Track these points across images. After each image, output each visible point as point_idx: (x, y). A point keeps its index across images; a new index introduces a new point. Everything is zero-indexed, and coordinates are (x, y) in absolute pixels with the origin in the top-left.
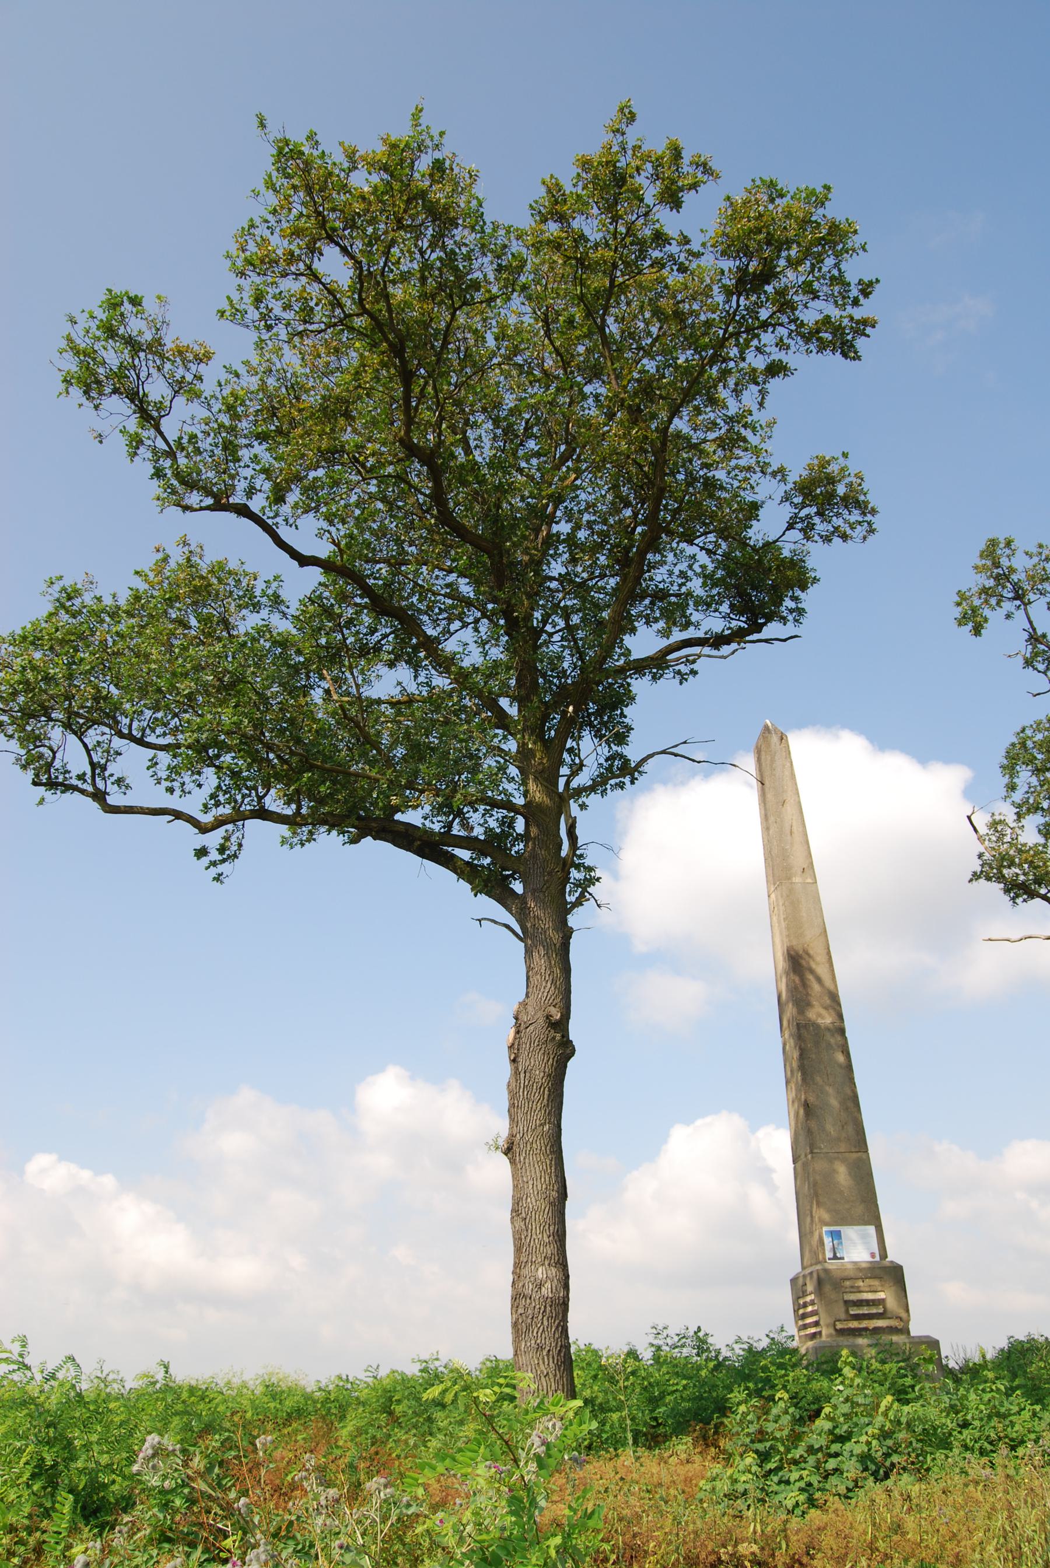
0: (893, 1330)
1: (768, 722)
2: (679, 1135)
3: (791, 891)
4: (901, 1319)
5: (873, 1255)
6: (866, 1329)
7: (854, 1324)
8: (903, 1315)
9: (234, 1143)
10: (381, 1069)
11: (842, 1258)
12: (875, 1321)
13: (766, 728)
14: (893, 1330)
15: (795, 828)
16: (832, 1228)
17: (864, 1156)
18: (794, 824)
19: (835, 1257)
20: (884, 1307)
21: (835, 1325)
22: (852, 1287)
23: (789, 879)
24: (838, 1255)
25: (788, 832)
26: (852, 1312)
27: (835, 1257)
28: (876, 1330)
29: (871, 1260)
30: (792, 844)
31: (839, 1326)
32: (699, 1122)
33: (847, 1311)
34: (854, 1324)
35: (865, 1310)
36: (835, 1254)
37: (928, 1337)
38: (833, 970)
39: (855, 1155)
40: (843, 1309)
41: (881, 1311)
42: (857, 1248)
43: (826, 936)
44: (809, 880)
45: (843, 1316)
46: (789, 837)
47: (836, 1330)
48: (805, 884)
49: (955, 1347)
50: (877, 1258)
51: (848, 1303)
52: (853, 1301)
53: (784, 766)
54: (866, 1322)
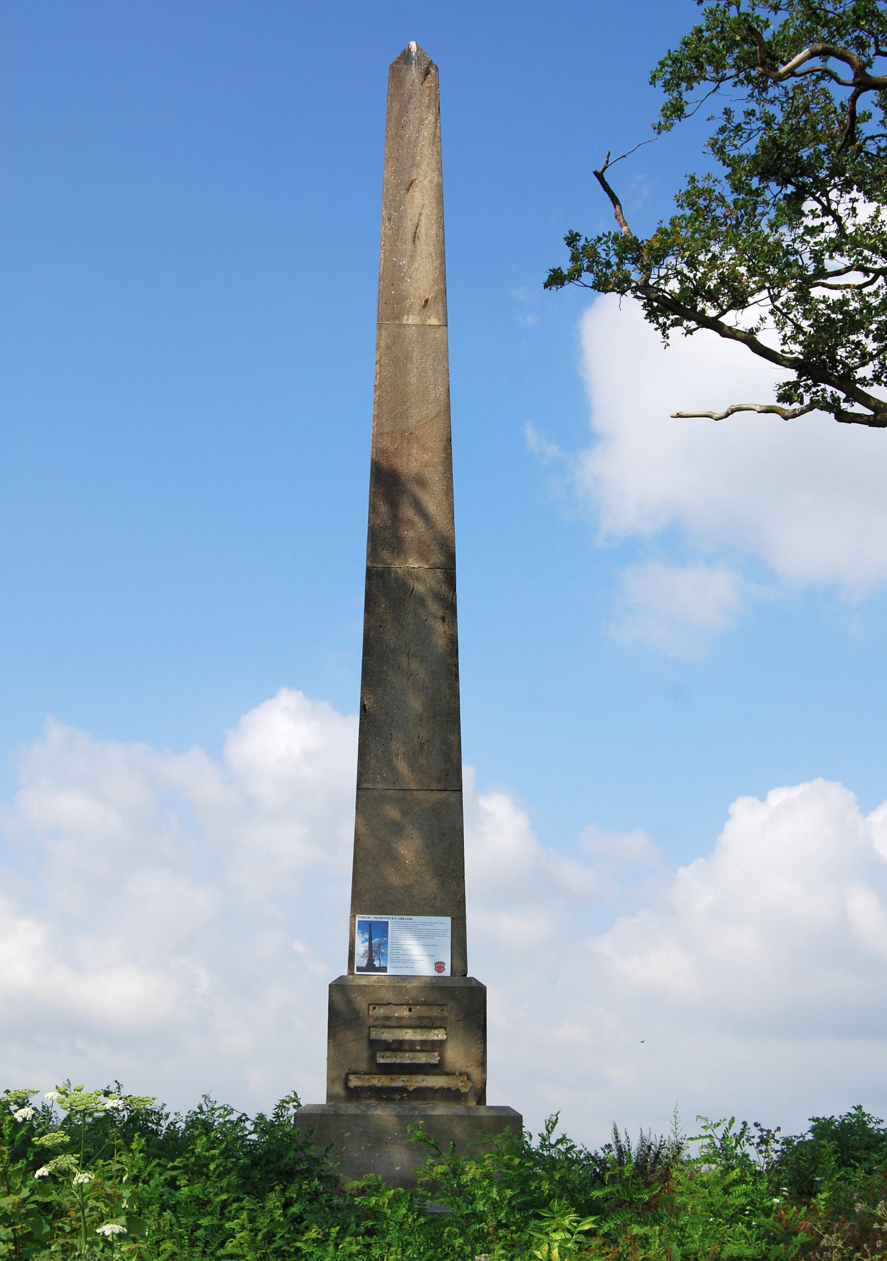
0: (451, 1095)
1: (413, 45)
2: (746, 818)
3: (396, 339)
4: (468, 1076)
5: (439, 966)
6: (402, 1090)
7: (378, 1081)
8: (474, 1071)
9: (71, 807)
10: (267, 693)
11: (384, 969)
12: (420, 1078)
13: (406, 56)
14: (451, 1095)
15: (422, 230)
16: (372, 918)
17: (453, 798)
18: (423, 223)
19: (370, 967)
20: (441, 1056)
21: (346, 1080)
22: (387, 1018)
23: (398, 317)
24: (377, 963)
25: (409, 237)
26: (381, 1061)
27: (370, 967)
28: (422, 1093)
29: (436, 974)
30: (412, 257)
31: (354, 1082)
32: (778, 797)
33: (372, 1058)
34: (378, 1081)
35: (406, 1058)
36: (371, 961)
37: (507, 1109)
38: (450, 478)
39: (436, 796)
40: (365, 1054)
41: (435, 1060)
42: (416, 951)
43: (449, 419)
44: (433, 321)
45: (363, 1066)
46: (409, 246)
47: (347, 1088)
48: (423, 327)
49: (623, 1139)
50: (447, 972)
51: (375, 1045)
52: (385, 1042)
53: (422, 121)
54: (405, 1078)
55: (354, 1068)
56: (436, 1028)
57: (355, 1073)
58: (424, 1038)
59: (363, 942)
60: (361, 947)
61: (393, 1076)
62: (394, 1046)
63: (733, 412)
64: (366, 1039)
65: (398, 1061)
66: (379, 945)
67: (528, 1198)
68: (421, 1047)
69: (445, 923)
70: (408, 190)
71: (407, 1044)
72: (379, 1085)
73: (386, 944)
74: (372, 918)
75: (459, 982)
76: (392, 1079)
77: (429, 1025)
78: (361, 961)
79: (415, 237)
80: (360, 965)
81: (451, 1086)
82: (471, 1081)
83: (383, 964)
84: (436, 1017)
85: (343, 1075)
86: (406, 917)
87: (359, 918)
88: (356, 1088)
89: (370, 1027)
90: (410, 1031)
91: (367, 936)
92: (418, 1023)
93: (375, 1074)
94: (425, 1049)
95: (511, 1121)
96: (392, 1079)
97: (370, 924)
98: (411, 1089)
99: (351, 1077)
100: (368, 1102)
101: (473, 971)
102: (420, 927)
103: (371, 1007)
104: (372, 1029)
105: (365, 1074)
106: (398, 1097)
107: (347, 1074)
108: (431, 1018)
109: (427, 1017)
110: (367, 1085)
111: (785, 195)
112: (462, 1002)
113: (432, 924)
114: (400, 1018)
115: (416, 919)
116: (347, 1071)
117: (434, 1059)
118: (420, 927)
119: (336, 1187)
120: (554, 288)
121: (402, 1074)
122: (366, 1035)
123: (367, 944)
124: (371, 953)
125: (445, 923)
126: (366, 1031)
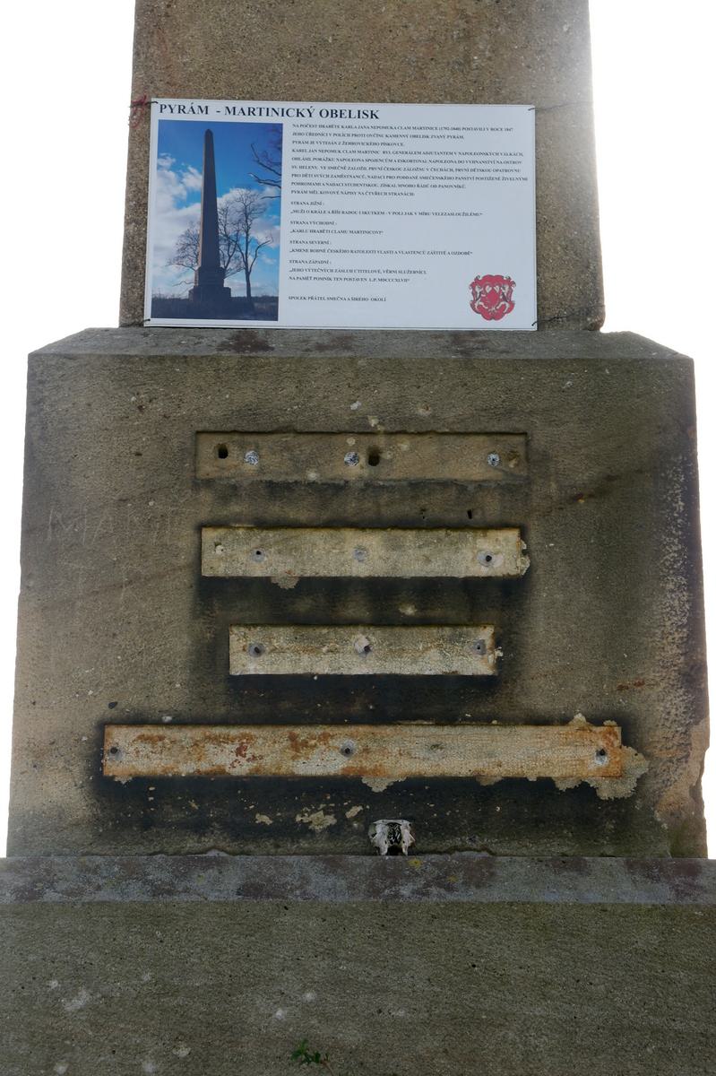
5: (492, 293)
16: (217, 111)
19: (210, 294)
21: (97, 751)
24: (235, 284)
26: (245, 664)
29: (478, 323)
31: (133, 757)
33: (212, 655)
36: (210, 274)
45: (173, 692)
47: (102, 786)
50: (522, 316)
55: (132, 700)
56: (487, 527)
57: (136, 720)
58: (436, 569)
59: (180, 203)
60: (171, 227)
61: (302, 732)
62: (303, 606)
64: (186, 578)
65: (321, 666)
66: (246, 214)
67: (118, 899)
68: (421, 607)
72: (243, 768)
73: (273, 208)
74: (392, 821)
75: (563, 343)
76: (297, 746)
77: (452, 516)
78: (171, 277)
80: (167, 291)
81: (555, 773)
82: (640, 749)
83: (259, 288)
84: (481, 485)
85: (86, 732)
86: (355, 107)
87: (163, 111)
88: (140, 783)
89: (200, 528)
90: (373, 542)
91: (195, 180)
92: (408, 509)
93: (225, 722)
94: (437, 613)
96: (297, 746)
97: (209, 134)
98: (379, 786)
99: (121, 737)
100: (191, 843)
101: (626, 310)
102: (410, 145)
103: (208, 447)
104: (209, 535)
105: (180, 722)
106: (320, 819)
107: (102, 725)
108: (461, 487)
109: (445, 484)
110: (186, 768)
113: (457, 132)
114: (337, 489)
115: (390, 113)
116: (101, 710)
117: (473, 658)
118: (410, 145)
119: (446, 1051)
121: (337, 721)
122: (183, 559)
123: (196, 210)
126: (185, 541)
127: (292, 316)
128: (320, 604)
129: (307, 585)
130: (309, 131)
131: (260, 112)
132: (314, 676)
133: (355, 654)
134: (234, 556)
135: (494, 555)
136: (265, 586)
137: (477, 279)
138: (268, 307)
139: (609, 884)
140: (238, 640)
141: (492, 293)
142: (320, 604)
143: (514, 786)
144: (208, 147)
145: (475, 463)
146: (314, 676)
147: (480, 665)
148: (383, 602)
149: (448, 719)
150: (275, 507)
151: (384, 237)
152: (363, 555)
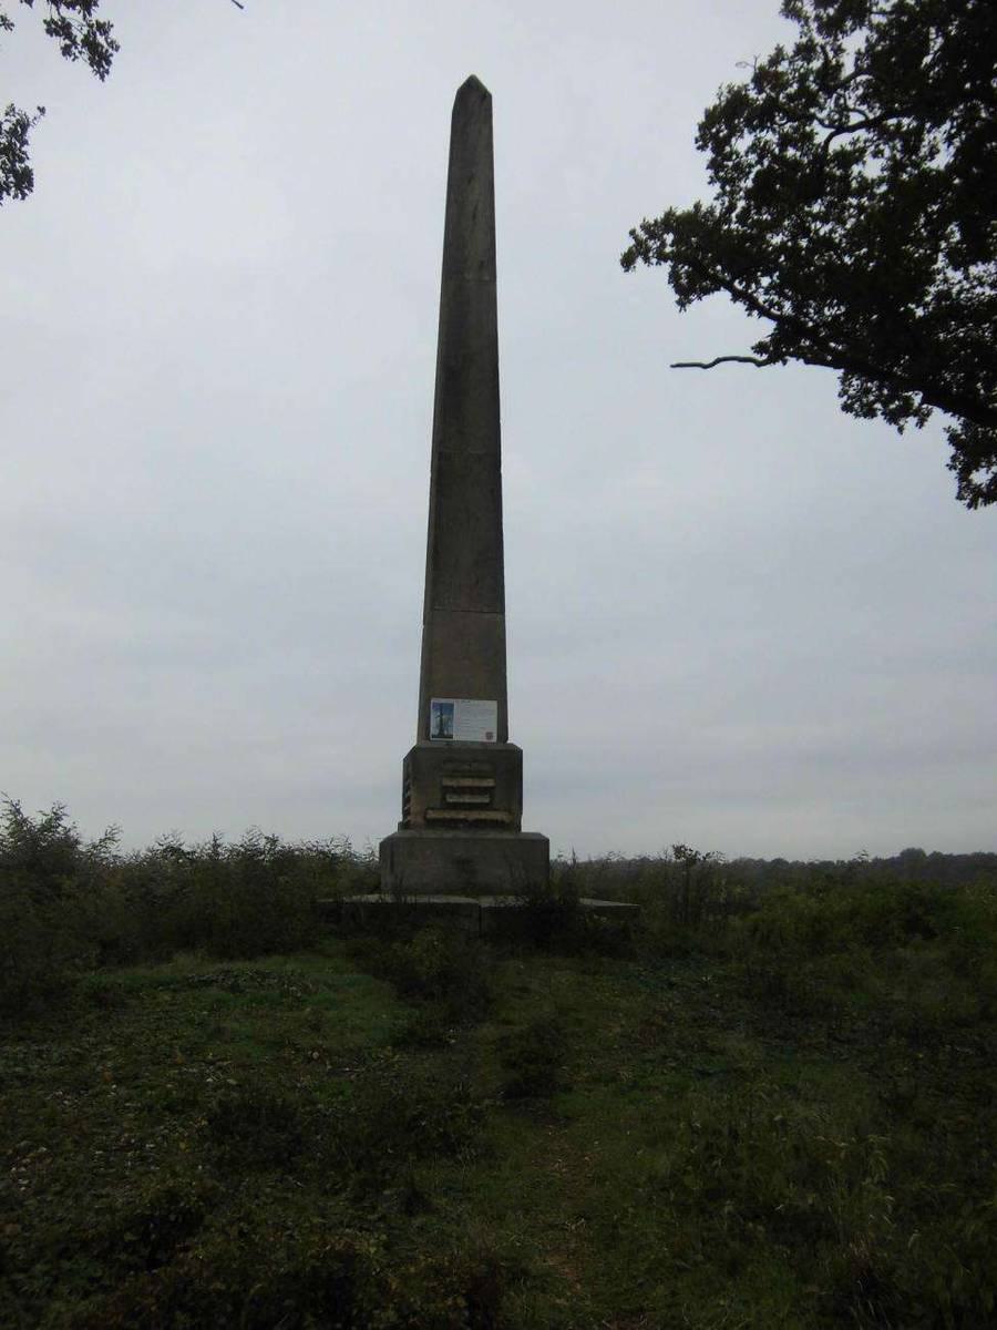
5: (489, 735)
7: (448, 815)
16: (443, 701)
19: (441, 735)
21: (426, 814)
24: (446, 732)
29: (485, 740)
31: (432, 815)
36: (441, 730)
50: (494, 739)
54: (467, 813)
55: (432, 806)
57: (432, 809)
63: (718, 361)
65: (461, 800)
69: (493, 705)
70: (469, 182)
71: (464, 781)
74: (443, 701)
75: (501, 746)
79: (474, 217)
95: (541, 844)
97: (441, 705)
99: (430, 812)
111: (749, 194)
112: (504, 765)
115: (472, 702)
117: (486, 800)
120: (728, 322)
124: (442, 726)
125: (493, 705)
127: (455, 738)
128: (461, 791)
129: (458, 787)
130: (459, 706)
131: (450, 701)
132: (932, 127)
133: (467, 799)
134: (448, 782)
135: (490, 783)
136: (452, 787)
137: (669, 215)
138: (451, 737)
139: (506, 835)
140: (448, 796)
141: (489, 735)
142: (461, 791)
143: (492, 821)
144: (441, 707)
145: (486, 767)
146: (932, 127)
147: (487, 801)
148: (472, 791)
149: (482, 810)
150: (453, 774)
151: (471, 724)
152: (468, 782)
